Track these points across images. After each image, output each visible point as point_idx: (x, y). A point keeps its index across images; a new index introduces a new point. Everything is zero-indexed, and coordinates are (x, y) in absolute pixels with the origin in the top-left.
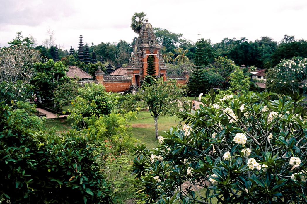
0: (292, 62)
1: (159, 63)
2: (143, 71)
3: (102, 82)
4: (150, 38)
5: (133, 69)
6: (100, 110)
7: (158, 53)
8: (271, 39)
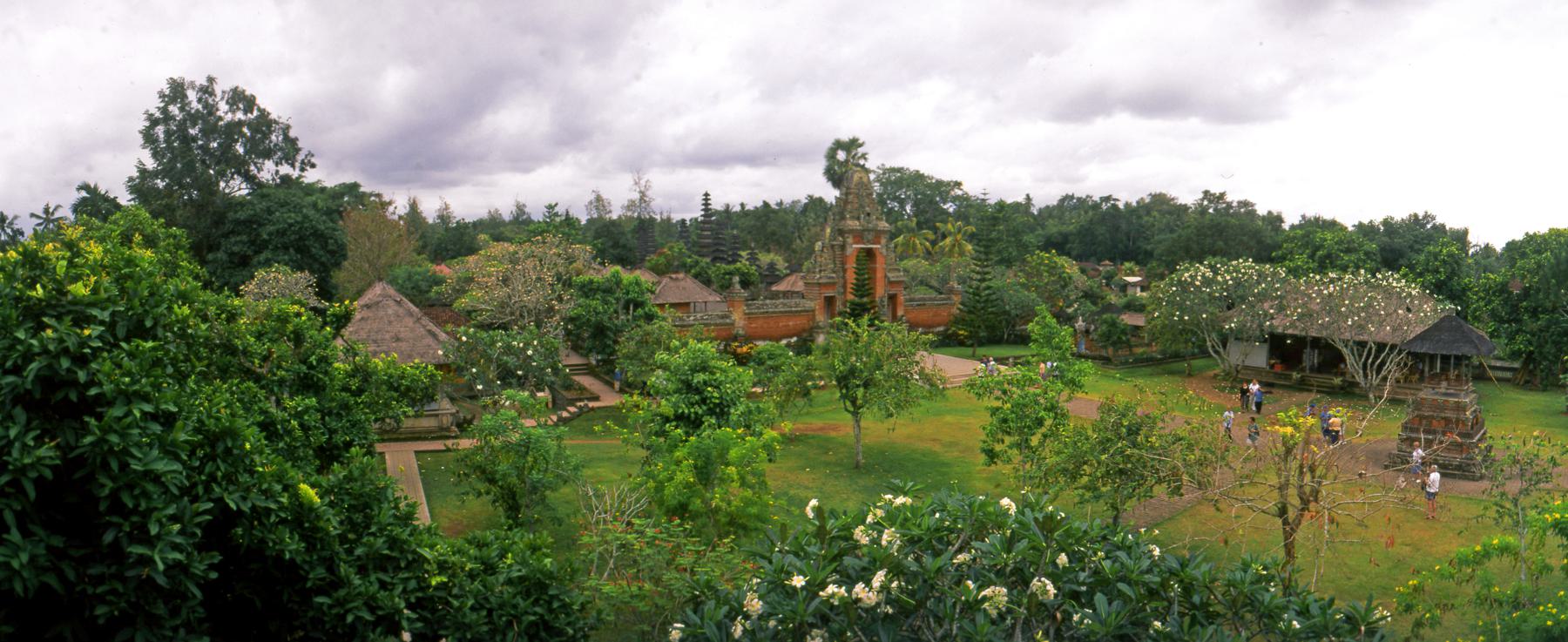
0: (1204, 270)
1: (884, 266)
2: (844, 286)
3: (741, 315)
4: (864, 207)
5: (819, 284)
6: (705, 408)
7: (883, 241)
8: (1173, 199)
